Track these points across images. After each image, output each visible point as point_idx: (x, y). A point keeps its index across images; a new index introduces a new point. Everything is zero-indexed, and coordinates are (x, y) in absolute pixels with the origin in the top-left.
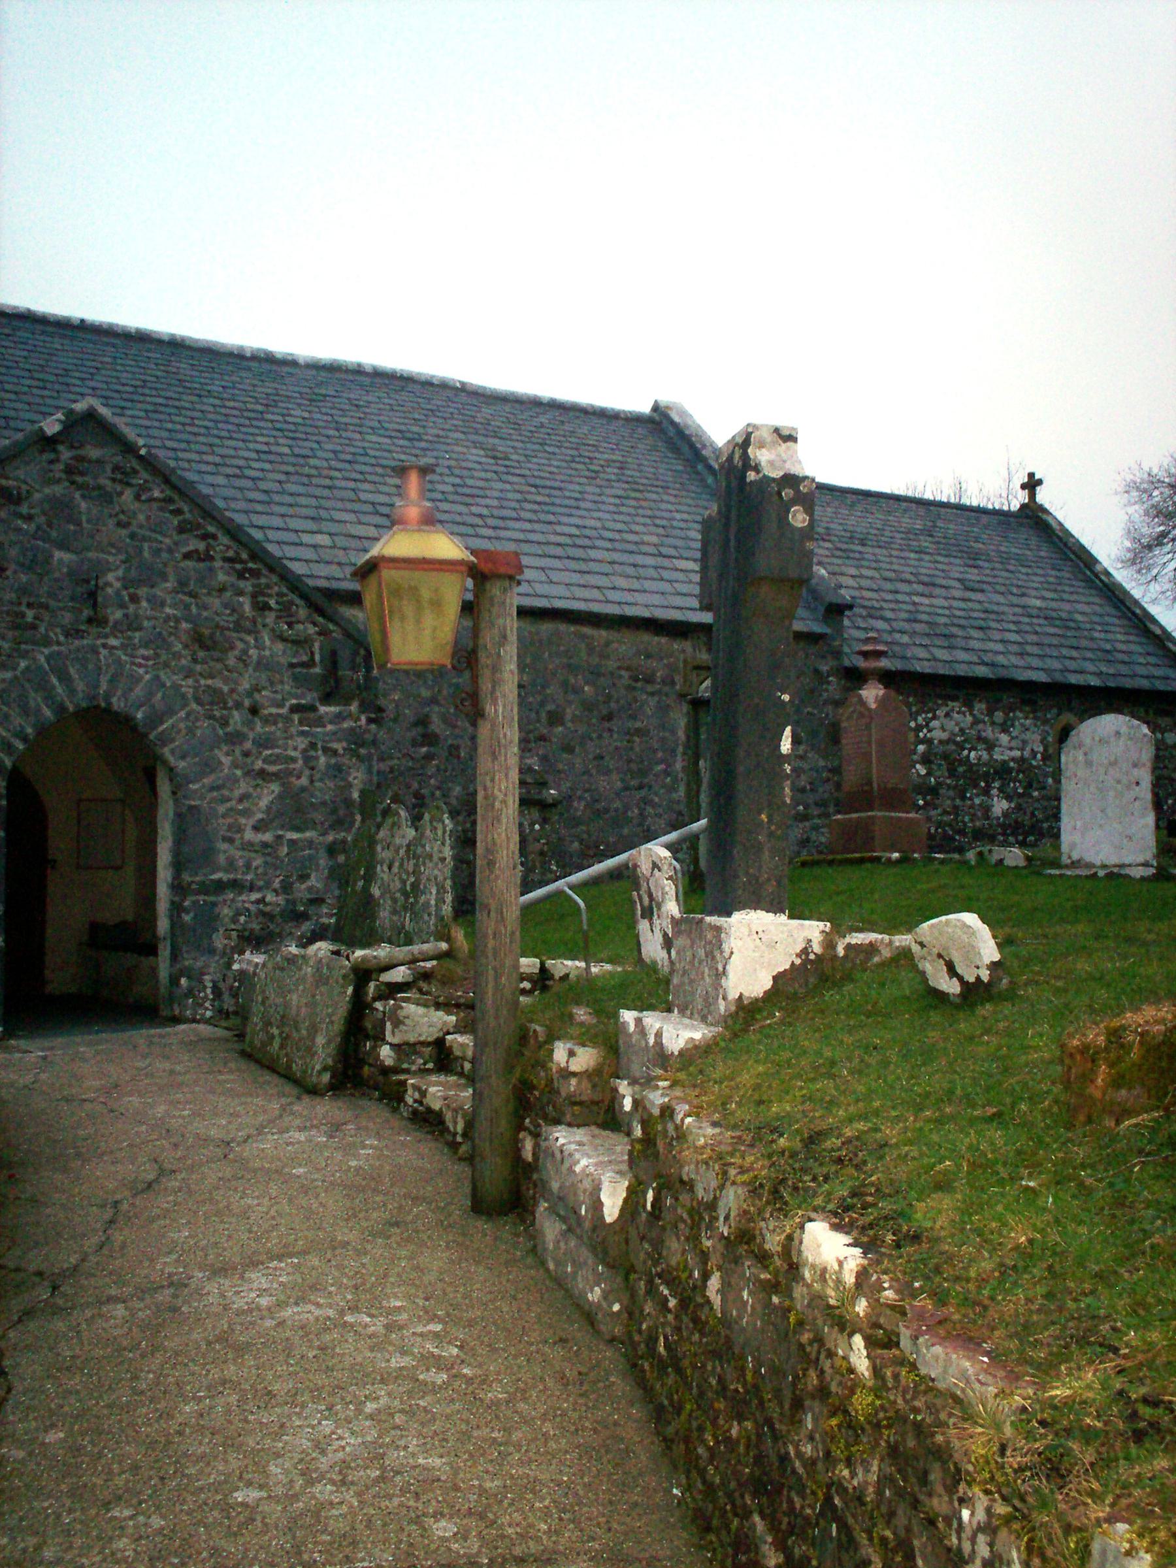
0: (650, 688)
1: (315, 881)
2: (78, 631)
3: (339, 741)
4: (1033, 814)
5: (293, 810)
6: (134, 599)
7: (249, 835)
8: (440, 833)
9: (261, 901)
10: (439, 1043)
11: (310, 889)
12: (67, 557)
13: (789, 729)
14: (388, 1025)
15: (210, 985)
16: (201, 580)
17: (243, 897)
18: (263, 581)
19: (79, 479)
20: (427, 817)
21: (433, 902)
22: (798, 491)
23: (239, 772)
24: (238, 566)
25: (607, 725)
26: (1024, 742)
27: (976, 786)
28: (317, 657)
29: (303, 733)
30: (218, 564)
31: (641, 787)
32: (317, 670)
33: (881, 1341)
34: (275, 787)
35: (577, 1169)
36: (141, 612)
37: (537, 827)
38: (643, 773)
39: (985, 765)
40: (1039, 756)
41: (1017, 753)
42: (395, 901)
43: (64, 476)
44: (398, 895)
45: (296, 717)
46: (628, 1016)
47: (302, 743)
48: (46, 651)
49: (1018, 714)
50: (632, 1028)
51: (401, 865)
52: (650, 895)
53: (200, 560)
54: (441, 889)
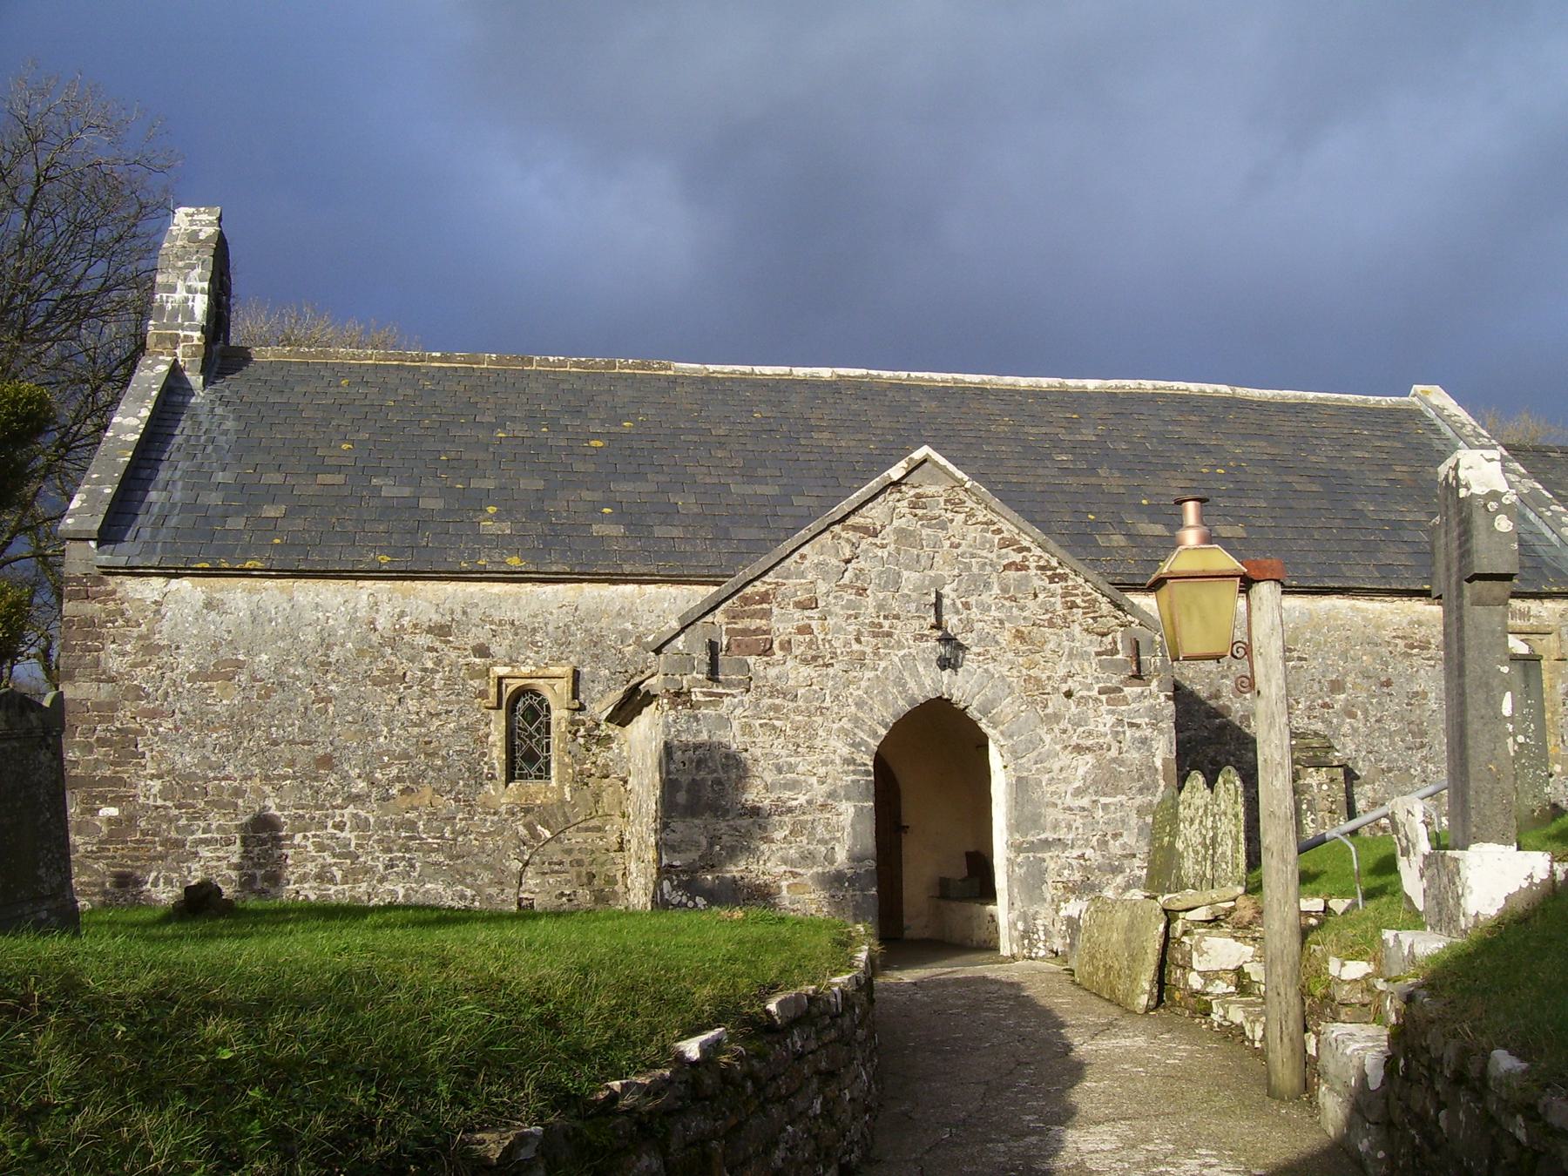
0: (1426, 654)
1: (1129, 838)
2: (923, 636)
5: (1107, 780)
6: (967, 606)
8: (1232, 792)
9: (1082, 856)
10: (1239, 971)
12: (915, 576)
13: (1508, 694)
14: (1195, 954)
16: (1017, 588)
18: (1070, 583)
19: (920, 512)
20: (1220, 780)
21: (1229, 853)
22: (1500, 503)
23: (1058, 747)
25: (1385, 690)
28: (1120, 646)
29: (1112, 712)
30: (1033, 572)
31: (1423, 746)
32: (1119, 656)
33: (1531, 1112)
35: (1348, 1052)
37: (1325, 787)
38: (1423, 734)
42: (1197, 853)
45: (1104, 698)
46: (1388, 935)
47: (1110, 720)
48: (902, 653)
50: (1391, 943)
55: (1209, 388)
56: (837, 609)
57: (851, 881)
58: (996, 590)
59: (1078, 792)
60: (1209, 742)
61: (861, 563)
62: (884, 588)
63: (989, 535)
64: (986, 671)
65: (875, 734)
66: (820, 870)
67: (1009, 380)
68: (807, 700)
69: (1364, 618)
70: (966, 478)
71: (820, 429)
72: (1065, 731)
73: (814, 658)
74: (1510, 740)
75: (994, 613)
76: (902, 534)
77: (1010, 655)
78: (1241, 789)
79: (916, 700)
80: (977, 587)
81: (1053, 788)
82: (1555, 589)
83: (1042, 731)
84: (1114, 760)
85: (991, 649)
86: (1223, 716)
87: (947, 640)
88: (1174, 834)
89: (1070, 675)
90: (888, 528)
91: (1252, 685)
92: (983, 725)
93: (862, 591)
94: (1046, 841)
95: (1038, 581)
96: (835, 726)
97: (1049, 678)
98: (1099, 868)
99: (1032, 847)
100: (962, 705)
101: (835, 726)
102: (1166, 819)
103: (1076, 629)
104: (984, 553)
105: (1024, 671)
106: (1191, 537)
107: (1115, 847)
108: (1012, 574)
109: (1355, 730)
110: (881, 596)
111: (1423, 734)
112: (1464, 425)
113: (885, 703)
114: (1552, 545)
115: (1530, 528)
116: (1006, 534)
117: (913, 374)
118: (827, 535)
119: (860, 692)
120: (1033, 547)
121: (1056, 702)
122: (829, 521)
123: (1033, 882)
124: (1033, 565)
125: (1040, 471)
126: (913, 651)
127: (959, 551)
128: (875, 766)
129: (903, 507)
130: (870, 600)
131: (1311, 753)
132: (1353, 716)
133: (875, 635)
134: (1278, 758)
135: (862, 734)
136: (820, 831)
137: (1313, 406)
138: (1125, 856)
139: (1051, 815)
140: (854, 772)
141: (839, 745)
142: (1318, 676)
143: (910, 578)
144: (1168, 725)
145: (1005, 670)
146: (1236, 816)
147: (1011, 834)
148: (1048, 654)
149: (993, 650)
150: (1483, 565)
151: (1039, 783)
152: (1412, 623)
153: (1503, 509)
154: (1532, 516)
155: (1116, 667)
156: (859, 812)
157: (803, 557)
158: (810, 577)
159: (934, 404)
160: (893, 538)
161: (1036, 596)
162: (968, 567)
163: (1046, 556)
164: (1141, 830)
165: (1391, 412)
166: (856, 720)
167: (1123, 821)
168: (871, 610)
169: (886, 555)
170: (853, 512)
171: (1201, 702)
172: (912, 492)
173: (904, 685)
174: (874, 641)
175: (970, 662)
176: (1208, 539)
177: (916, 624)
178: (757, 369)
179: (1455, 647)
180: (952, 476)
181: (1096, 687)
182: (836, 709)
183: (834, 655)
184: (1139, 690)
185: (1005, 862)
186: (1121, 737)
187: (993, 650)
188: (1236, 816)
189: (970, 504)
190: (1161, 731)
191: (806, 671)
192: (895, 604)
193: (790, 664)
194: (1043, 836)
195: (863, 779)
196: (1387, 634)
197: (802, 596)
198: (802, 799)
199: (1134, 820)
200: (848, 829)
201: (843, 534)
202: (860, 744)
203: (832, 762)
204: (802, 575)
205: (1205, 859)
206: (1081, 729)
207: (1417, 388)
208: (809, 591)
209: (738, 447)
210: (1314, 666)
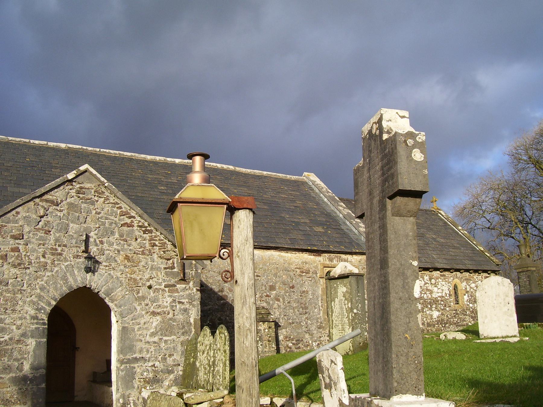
0: (308, 275)
2: (78, 256)
3: (184, 299)
4: (447, 316)
5: (166, 329)
6: (102, 242)
7: (148, 338)
8: (223, 339)
11: (174, 360)
15: (132, 402)
16: (128, 235)
17: (146, 364)
18: (153, 234)
19: (81, 196)
20: (218, 332)
21: (221, 371)
24: (143, 229)
25: (292, 290)
26: (442, 290)
27: (427, 307)
28: (175, 265)
29: (170, 296)
30: (135, 228)
31: (306, 313)
32: (175, 270)
34: (159, 318)
36: (104, 247)
37: (267, 330)
39: (430, 299)
40: (448, 295)
41: (440, 294)
43: (75, 194)
44: (207, 366)
45: (167, 289)
47: (170, 300)
48: (67, 264)
49: (439, 280)
51: (208, 353)
52: (330, 377)
53: (128, 227)
54: (225, 365)
55: (225, 167)
56: (34, 240)
57: (31, 380)
58: (117, 236)
59: (153, 335)
60: (216, 312)
61: (49, 219)
62: (60, 231)
63: (115, 209)
64: (110, 274)
65: (49, 304)
66: (14, 375)
67: (143, 156)
68: (13, 285)
69: (284, 260)
70: (106, 181)
71: (56, 168)
72: (147, 305)
73: (19, 264)
74: (419, 316)
75: (115, 246)
76: (71, 206)
77: (122, 267)
78: (228, 337)
79: (72, 287)
80: (107, 234)
81: (140, 332)
82: (357, 251)
83: (136, 305)
84: (171, 319)
85: (113, 264)
86: (224, 299)
87: (90, 258)
88: (195, 358)
89: (151, 278)
90: (64, 202)
91: (232, 277)
92: (107, 300)
93: (48, 232)
94: (136, 358)
95: (138, 233)
96: (28, 299)
97: (141, 279)
98: (162, 371)
99: (129, 361)
100: (96, 291)
101: (28, 299)
102: (191, 349)
103: (155, 256)
104: (112, 218)
105: (129, 275)
106: (196, 178)
107: (170, 361)
108: (125, 228)
109: (279, 306)
110: (58, 235)
111: (306, 308)
112: (323, 188)
113: (56, 289)
114: (355, 234)
115: (347, 227)
116: (124, 210)
117: (102, 150)
118: (32, 203)
119: (43, 283)
120: (136, 216)
121: (143, 291)
122: (33, 196)
123: (128, 379)
124: (136, 225)
125: (151, 193)
126: (73, 263)
127: (100, 216)
128: (48, 320)
129: (73, 192)
130: (52, 237)
131: (262, 316)
132: (279, 300)
133: (53, 254)
134: (248, 325)
135: (42, 304)
136: (16, 354)
137: (266, 177)
138: (175, 365)
139: (139, 345)
140: (37, 323)
141: (30, 309)
142: (264, 283)
143: (73, 227)
144: (197, 303)
145: (119, 274)
146: (225, 351)
147: (118, 355)
148: (141, 267)
149: (113, 265)
150: (405, 184)
151: (133, 330)
152: (303, 263)
153: (417, 145)
154: (348, 223)
155: (174, 275)
156: (38, 344)
157: (18, 213)
158: (21, 223)
159: (109, 163)
160: (66, 207)
161: (136, 239)
162: (104, 224)
163: (143, 221)
164: (182, 352)
165: (295, 182)
166: (40, 297)
167: (174, 348)
168: (52, 242)
169: (62, 215)
170: (46, 193)
171: (215, 293)
172: (78, 186)
173: (67, 280)
174: (52, 257)
175: (102, 270)
176: (207, 181)
177: (75, 250)
178: (32, 141)
179: (377, 247)
180: (99, 179)
181: (164, 284)
182: (29, 291)
183: (30, 263)
184: (184, 286)
185: (115, 368)
186: (174, 308)
187: (113, 265)
188: (225, 351)
189: (107, 194)
190: (194, 306)
191: (14, 271)
192: (65, 240)
193: (5, 267)
194: (134, 356)
195: (41, 327)
196: (293, 267)
197: (15, 232)
198: (7, 337)
199: (179, 348)
200: (31, 353)
201: (40, 203)
202: (41, 309)
203: (25, 318)
204: (16, 222)
205: (209, 372)
206: (155, 304)
207: (306, 174)
208: (19, 230)
209: (15, 172)
210: (263, 279)
